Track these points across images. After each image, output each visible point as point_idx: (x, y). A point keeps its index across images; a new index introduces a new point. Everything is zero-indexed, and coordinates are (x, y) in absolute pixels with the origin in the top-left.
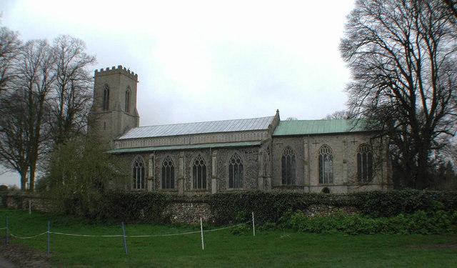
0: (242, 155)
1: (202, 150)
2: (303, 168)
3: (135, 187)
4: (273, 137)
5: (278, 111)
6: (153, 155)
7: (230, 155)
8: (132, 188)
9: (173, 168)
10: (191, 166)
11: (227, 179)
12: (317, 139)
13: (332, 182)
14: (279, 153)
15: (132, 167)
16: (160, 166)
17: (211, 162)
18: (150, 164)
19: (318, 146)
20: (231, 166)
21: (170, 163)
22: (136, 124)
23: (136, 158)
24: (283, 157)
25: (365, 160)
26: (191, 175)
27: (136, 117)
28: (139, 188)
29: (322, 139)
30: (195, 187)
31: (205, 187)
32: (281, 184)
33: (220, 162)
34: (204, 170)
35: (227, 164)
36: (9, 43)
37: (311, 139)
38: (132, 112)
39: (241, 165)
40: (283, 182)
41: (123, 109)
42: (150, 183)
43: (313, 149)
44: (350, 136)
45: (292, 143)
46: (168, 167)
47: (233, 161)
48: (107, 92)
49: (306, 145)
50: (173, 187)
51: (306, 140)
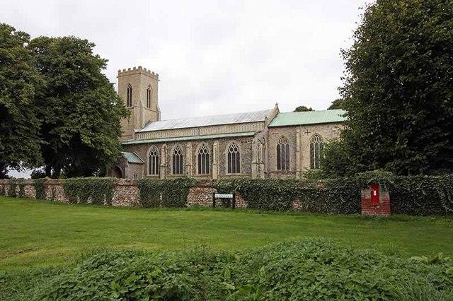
3: (150, 173)
4: (269, 128)
5: (277, 104)
6: (164, 145)
8: (148, 173)
9: (208, 155)
12: (309, 128)
14: (274, 143)
15: (148, 155)
16: (172, 155)
17: (160, 152)
18: (163, 153)
20: (229, 154)
21: (236, 150)
23: (151, 147)
24: (278, 146)
26: (197, 161)
27: (158, 112)
28: (154, 173)
30: (200, 172)
31: (208, 172)
32: (276, 169)
33: (222, 151)
35: (226, 153)
37: (302, 129)
38: (153, 108)
39: (238, 153)
41: (144, 105)
42: (163, 171)
45: (286, 133)
49: (298, 135)
51: (298, 130)
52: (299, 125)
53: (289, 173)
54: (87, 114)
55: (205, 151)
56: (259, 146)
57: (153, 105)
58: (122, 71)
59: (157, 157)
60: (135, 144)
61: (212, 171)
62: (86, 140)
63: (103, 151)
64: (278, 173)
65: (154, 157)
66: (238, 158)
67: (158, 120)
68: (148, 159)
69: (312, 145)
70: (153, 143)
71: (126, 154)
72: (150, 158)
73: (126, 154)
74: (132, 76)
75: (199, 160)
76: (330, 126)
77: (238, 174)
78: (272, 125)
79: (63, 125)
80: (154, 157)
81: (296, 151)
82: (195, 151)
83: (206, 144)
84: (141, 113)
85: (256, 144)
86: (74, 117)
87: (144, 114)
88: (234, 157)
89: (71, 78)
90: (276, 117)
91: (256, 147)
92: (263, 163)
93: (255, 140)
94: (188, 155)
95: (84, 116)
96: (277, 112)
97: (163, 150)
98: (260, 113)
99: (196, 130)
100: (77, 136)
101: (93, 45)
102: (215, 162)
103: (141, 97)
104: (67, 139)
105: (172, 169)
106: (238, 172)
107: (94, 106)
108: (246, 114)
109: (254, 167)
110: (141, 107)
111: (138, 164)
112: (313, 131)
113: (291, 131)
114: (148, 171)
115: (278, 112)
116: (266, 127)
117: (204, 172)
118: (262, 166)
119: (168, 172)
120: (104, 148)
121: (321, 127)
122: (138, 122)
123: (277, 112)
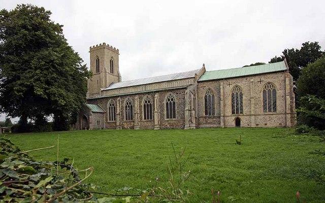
0: (174, 95)
1: (148, 93)
2: (220, 103)
4: (198, 82)
5: (204, 65)
7: (167, 95)
10: (143, 104)
11: (165, 112)
12: (230, 81)
13: (242, 113)
15: (108, 107)
17: (116, 103)
18: (118, 104)
19: (231, 87)
20: (167, 104)
21: (172, 99)
22: (119, 80)
23: (127, 99)
24: (206, 96)
25: (270, 95)
26: (143, 110)
27: (119, 76)
28: (112, 120)
29: (234, 81)
30: (145, 118)
31: (151, 118)
33: (161, 101)
34: (151, 106)
35: (165, 102)
36: (303, 82)
37: (225, 82)
38: (115, 73)
39: (174, 103)
40: (206, 114)
41: (108, 70)
42: (118, 118)
43: (227, 90)
44: (257, 77)
45: (212, 86)
46: (171, 103)
47: (169, 100)
48: (98, 61)
49: (221, 87)
50: (132, 119)
52: (222, 79)
53: (214, 117)
54: (41, 70)
55: (149, 102)
56: (190, 96)
57: (115, 71)
58: (92, 47)
59: (114, 108)
60: (99, 99)
61: (154, 117)
62: (39, 91)
63: (56, 101)
64: (205, 118)
65: (112, 108)
66: (174, 107)
67: (119, 81)
68: (108, 109)
69: (233, 95)
70: (111, 97)
71: (90, 106)
72: (110, 108)
73: (90, 106)
74: (98, 51)
75: (145, 108)
76: (248, 78)
77: (174, 119)
78: (201, 80)
79: (19, 79)
80: (112, 108)
81: (220, 99)
82: (141, 102)
83: (150, 96)
84: (106, 76)
85: (188, 95)
86: (29, 72)
87: (108, 78)
88: (148, 108)
89: (26, 38)
90: (203, 74)
91: (188, 96)
92: (194, 110)
93: (187, 91)
94: (136, 106)
95: (38, 71)
96: (204, 71)
97: (118, 102)
98: (192, 72)
99: (144, 87)
100: (31, 88)
101: (49, 13)
102: (156, 110)
103: (106, 65)
104: (22, 91)
105: (125, 116)
106: (174, 117)
107: (48, 63)
108: (181, 73)
109: (187, 113)
110: (106, 72)
111: (101, 113)
112: (233, 83)
113: (216, 84)
114: (108, 118)
115: (205, 71)
116: (196, 82)
117: (148, 119)
118: (193, 112)
119: (123, 119)
120: (58, 99)
121: (240, 79)
122: (104, 82)
123: (204, 71)
